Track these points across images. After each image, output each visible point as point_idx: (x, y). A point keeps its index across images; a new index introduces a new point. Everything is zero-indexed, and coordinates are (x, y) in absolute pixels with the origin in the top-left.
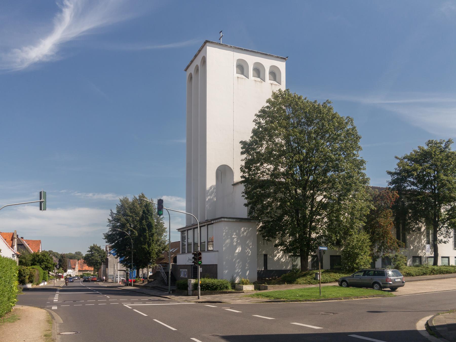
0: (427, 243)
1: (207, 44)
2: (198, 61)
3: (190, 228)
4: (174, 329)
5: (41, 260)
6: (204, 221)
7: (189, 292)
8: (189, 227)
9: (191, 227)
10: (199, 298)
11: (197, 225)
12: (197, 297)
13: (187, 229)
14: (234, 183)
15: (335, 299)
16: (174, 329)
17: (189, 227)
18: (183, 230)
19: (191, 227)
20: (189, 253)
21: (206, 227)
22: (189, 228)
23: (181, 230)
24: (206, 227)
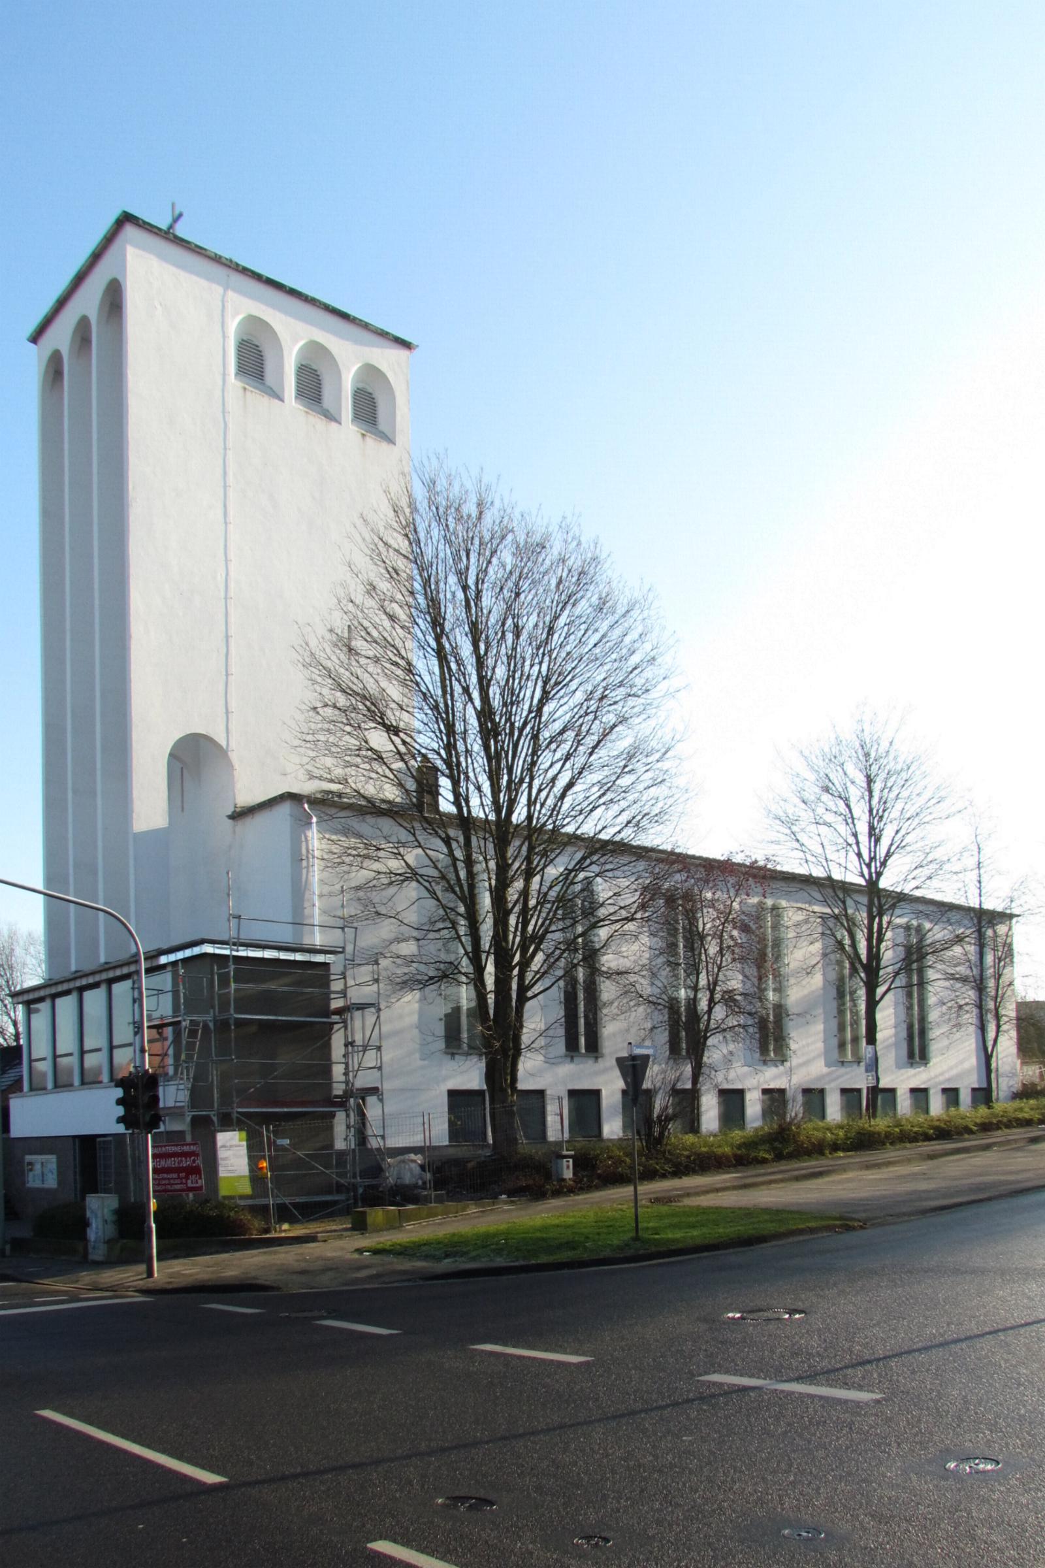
0: (595, 1054)
1: (129, 230)
2: (88, 301)
3: (65, 987)
4: (47, 1413)
5: (771, 1017)
6: (67, 975)
7: (90, 1250)
8: (62, 982)
9: (71, 985)
10: (150, 1273)
11: (137, 962)
12: (142, 1268)
13: (53, 990)
14: (238, 810)
15: (673, 1262)
16: (47, 1413)
17: (62, 982)
18: (36, 995)
19: (71, 985)
20: (86, 1086)
21: (103, 988)
22: (60, 988)
23: (26, 997)
24: (103, 988)
